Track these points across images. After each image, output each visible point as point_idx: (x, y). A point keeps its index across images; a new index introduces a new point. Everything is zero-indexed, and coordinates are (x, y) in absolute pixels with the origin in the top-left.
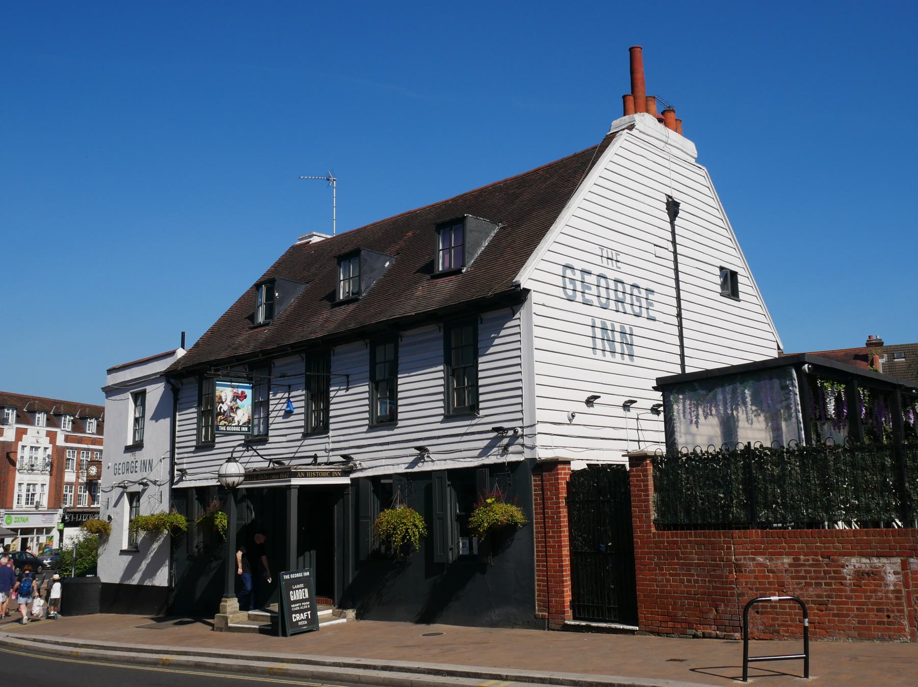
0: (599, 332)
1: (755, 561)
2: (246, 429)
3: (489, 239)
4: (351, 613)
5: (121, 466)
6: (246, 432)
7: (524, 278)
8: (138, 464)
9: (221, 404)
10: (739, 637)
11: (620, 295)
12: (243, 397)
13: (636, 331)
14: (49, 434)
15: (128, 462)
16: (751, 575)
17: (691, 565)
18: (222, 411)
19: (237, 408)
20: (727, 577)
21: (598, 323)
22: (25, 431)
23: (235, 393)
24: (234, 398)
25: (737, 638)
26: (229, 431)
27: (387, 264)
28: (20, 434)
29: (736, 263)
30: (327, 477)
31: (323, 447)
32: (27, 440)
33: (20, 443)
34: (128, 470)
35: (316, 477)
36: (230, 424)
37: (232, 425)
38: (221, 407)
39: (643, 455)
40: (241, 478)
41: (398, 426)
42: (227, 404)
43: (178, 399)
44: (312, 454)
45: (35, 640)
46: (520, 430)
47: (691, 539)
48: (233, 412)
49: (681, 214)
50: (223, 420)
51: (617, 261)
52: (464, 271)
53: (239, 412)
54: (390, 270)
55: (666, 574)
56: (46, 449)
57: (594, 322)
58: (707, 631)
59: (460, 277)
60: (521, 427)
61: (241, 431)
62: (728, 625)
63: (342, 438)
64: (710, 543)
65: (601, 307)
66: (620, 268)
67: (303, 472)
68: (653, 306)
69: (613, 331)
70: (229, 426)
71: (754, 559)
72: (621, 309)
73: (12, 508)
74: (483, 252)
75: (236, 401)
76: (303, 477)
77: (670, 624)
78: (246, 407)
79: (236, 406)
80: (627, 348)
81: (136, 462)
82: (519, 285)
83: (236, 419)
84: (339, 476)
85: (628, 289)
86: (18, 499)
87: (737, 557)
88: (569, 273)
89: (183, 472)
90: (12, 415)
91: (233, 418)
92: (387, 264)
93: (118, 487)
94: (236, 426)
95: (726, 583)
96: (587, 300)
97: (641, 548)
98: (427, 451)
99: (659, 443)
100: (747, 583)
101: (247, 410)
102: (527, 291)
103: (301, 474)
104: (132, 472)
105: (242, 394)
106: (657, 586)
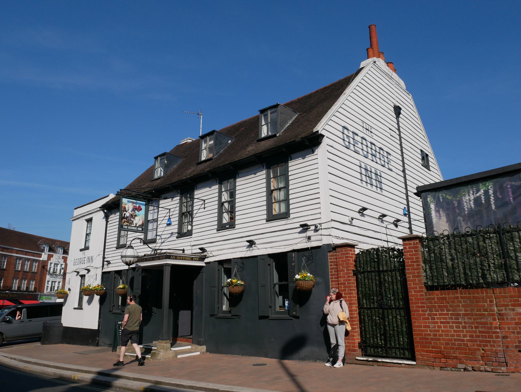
0: (363, 172)
1: (514, 311)
2: (141, 229)
3: (292, 120)
4: (204, 348)
5: (77, 260)
6: (140, 231)
7: (320, 128)
8: (86, 259)
9: (125, 212)
10: (505, 370)
11: (374, 152)
12: (139, 209)
13: (383, 175)
14: (63, 258)
15: (81, 258)
16: (512, 322)
17: (459, 315)
18: (126, 216)
19: (136, 216)
20: (491, 324)
21: (363, 165)
22: (52, 256)
23: (134, 206)
24: (134, 209)
25: (504, 372)
26: (129, 229)
27: (230, 141)
28: (50, 257)
29: (428, 150)
30: (190, 260)
31: (189, 244)
32: (53, 260)
33: (49, 261)
34: (80, 262)
35: (183, 260)
36: (130, 225)
37: (132, 225)
38: (125, 214)
39: (163, 390)
40: (135, 259)
41: (235, 228)
42: (129, 213)
43: (108, 222)
44: (182, 248)
45: (22, 361)
46: (319, 226)
47: (457, 295)
48: (133, 218)
49: (401, 116)
50: (126, 222)
51: (371, 132)
52: (278, 135)
53: (137, 218)
54: (231, 145)
55: (437, 323)
56: (62, 265)
57: (361, 164)
58: (476, 365)
59: (275, 138)
60: (319, 224)
61: (137, 230)
62: (495, 361)
63: (200, 238)
64: (474, 298)
65: (364, 157)
66: (372, 136)
67: (174, 256)
68: (391, 163)
69: (371, 172)
70: (130, 226)
71: (513, 310)
72: (375, 160)
73: (44, 292)
74: (289, 126)
75: (135, 211)
76: (174, 259)
77: (443, 360)
78: (141, 215)
79: (135, 214)
80: (379, 183)
81: (85, 258)
82: (318, 132)
83: (135, 222)
84: (198, 261)
85: (378, 150)
86: (47, 288)
87: (499, 308)
88: (346, 132)
89: (109, 263)
90: (47, 249)
91: (133, 222)
92: (230, 141)
93: (75, 272)
94: (134, 227)
95: (491, 328)
96: (357, 150)
97: (415, 303)
98: (254, 243)
99: (398, 244)
100: (509, 328)
101: (142, 217)
102: (323, 136)
103: (173, 257)
104: (82, 264)
105: (139, 207)
106: (430, 331)
